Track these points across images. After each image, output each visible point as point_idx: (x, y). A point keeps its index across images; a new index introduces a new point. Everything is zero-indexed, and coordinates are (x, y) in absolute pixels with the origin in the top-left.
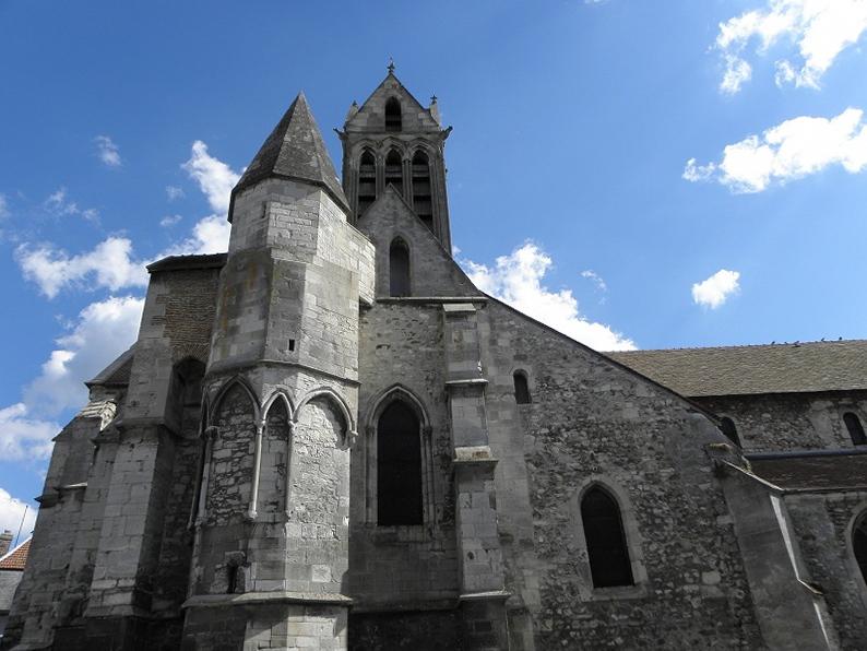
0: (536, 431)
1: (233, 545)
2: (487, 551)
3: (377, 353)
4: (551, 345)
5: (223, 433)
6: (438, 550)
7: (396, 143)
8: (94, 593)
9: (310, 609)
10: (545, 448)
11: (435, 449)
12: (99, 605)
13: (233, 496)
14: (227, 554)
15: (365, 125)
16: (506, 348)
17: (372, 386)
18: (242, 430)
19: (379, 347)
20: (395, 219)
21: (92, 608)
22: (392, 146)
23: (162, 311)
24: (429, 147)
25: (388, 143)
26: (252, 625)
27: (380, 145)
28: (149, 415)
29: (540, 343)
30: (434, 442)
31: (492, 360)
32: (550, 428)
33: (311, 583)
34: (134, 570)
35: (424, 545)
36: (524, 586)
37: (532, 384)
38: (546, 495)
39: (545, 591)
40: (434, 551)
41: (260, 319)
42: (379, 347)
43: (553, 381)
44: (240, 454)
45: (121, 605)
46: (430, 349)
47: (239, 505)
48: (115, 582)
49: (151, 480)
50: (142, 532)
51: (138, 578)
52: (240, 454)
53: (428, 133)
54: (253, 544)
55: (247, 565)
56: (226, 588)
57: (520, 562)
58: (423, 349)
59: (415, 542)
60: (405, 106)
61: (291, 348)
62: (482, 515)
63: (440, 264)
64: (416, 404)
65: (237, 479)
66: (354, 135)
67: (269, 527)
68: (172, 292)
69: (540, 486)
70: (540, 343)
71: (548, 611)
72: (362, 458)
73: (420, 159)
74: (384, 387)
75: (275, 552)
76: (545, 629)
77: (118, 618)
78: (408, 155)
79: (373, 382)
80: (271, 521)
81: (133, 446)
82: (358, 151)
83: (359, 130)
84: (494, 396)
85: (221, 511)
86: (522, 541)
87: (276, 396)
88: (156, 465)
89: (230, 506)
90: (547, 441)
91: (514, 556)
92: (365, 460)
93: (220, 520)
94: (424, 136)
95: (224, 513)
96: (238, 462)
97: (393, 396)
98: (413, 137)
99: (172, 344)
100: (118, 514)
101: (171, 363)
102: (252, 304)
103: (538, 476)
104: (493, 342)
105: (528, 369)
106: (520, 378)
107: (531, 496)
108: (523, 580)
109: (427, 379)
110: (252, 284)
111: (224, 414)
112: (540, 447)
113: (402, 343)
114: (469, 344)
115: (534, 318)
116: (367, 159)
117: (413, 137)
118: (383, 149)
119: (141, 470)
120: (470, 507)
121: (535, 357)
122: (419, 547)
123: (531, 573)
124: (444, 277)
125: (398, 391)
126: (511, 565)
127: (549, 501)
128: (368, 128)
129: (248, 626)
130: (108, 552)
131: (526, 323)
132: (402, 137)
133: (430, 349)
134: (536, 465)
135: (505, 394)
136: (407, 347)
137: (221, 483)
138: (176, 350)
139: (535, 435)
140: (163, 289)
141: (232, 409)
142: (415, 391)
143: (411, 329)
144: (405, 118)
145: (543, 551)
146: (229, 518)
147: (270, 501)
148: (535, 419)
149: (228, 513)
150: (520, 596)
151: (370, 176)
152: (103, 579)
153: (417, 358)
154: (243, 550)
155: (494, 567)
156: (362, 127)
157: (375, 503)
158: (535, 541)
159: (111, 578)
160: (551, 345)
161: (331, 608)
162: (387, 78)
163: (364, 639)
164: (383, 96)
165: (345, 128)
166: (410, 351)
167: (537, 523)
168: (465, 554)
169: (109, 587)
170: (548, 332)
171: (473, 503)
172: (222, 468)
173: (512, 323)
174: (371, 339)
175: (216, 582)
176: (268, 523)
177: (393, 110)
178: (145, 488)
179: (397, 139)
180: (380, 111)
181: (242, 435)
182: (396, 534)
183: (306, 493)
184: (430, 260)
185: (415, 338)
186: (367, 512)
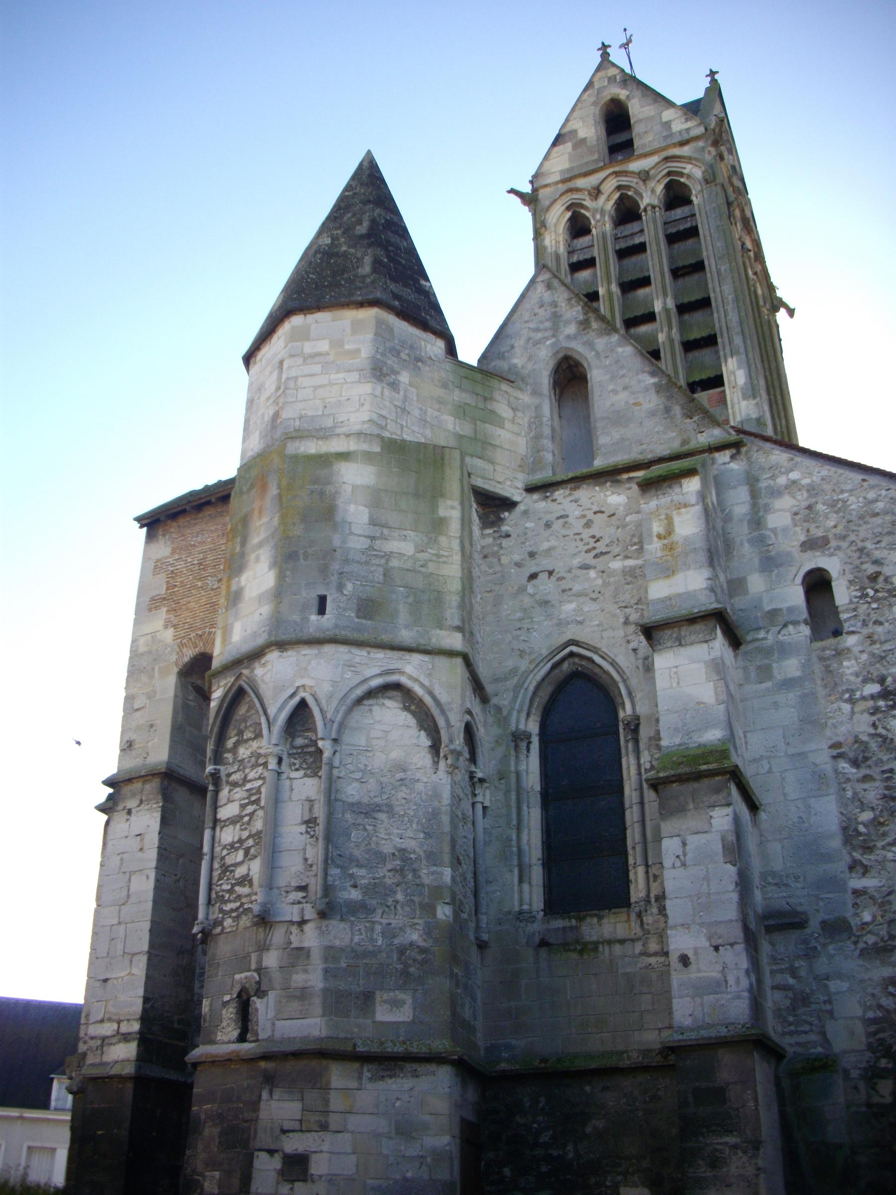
0: (852, 692)
1: (242, 963)
2: (716, 948)
3: (530, 590)
4: (880, 505)
5: (229, 775)
6: (655, 954)
7: (624, 180)
8: (92, 1043)
9: (374, 1067)
10: (874, 725)
11: (645, 758)
12: (98, 1061)
13: (246, 880)
14: (237, 977)
15: (566, 165)
16: (785, 530)
17: (522, 653)
18: (253, 767)
19: (533, 576)
20: (555, 329)
21: (92, 1065)
22: (619, 188)
23: (160, 587)
24: (688, 168)
25: (610, 186)
26: (271, 1092)
27: (596, 192)
28: (148, 761)
29: (855, 504)
30: (642, 745)
31: (756, 561)
32: (882, 680)
33: (374, 1022)
34: (137, 1007)
35: (628, 945)
36: (831, 1012)
37: (842, 594)
38: (876, 823)
39: (874, 1021)
40: (650, 955)
41: (270, 569)
42: (533, 576)
43: (886, 580)
44: (250, 809)
45: (123, 1061)
46: (630, 563)
47: (249, 895)
48: (115, 1026)
49: (153, 864)
50: (146, 948)
51: (145, 1018)
52: (250, 809)
53: (682, 144)
54: (271, 960)
55: (261, 993)
56: (235, 1034)
57: (822, 965)
58: (616, 565)
59: (610, 942)
60: (637, 109)
61: (322, 611)
62: (707, 878)
63: (646, 389)
64: (607, 673)
65: (247, 851)
66: (548, 190)
67: (294, 929)
68: (173, 552)
69: (863, 807)
70: (855, 504)
71: (883, 1063)
72: (507, 792)
73: (676, 196)
74: (545, 652)
75: (306, 971)
76: (876, 1099)
77: (120, 1078)
78: (650, 196)
79: (522, 646)
80: (296, 918)
81: (129, 812)
82: (558, 217)
83: (557, 178)
84: (762, 634)
85: (228, 907)
86: (824, 923)
87: (296, 700)
88: (161, 839)
89: (239, 897)
90: (876, 711)
91: (810, 954)
92: (513, 796)
93: (228, 922)
94: (677, 151)
95: (232, 910)
96: (249, 823)
97: (565, 666)
98: (655, 159)
99: (176, 638)
100: (116, 921)
101: (176, 670)
102: (260, 545)
103: (860, 787)
104: (756, 521)
105: (832, 565)
106: (818, 585)
107: (845, 829)
108: (829, 1001)
109: (626, 622)
110: (260, 512)
111: (230, 743)
112: (862, 725)
113: (576, 562)
114: (686, 539)
115: (843, 457)
116: (578, 227)
117: (655, 159)
118: (602, 199)
119: (141, 849)
120: (684, 865)
121: (843, 538)
122: (617, 948)
123: (845, 985)
124: (653, 414)
125: (572, 654)
126: (803, 973)
127: (884, 834)
128: (572, 169)
129: (265, 1095)
130: (106, 981)
131: (827, 470)
132: (635, 166)
133: (630, 563)
134: (855, 763)
135: (785, 625)
136: (586, 567)
137: (229, 860)
138: (181, 645)
139: (851, 701)
140: (163, 549)
141: (240, 733)
142: (603, 646)
143: (592, 531)
144: (638, 129)
145: (871, 939)
146: (238, 917)
147: (294, 884)
148: (849, 667)
149: (237, 909)
150: (824, 1034)
151: (688, 225)
152: (102, 1021)
153: (606, 584)
154: (255, 971)
155: (731, 980)
156: (561, 172)
157: (537, 874)
158: (854, 922)
159: (110, 1020)
160: (880, 505)
161: (415, 1066)
162: (598, 69)
163: (519, 1119)
164: (595, 104)
165: (531, 182)
166: (592, 574)
167: (857, 883)
168: (674, 958)
169: (109, 1033)
170: (873, 480)
171: (690, 855)
172: (228, 835)
173: (794, 475)
174: (518, 565)
175: (224, 1024)
176: (292, 923)
177: (616, 120)
178: (148, 877)
179: (625, 173)
180: (590, 130)
181: (251, 776)
182: (577, 928)
183: (360, 866)
184: (625, 388)
185: (601, 547)
186: (521, 892)
